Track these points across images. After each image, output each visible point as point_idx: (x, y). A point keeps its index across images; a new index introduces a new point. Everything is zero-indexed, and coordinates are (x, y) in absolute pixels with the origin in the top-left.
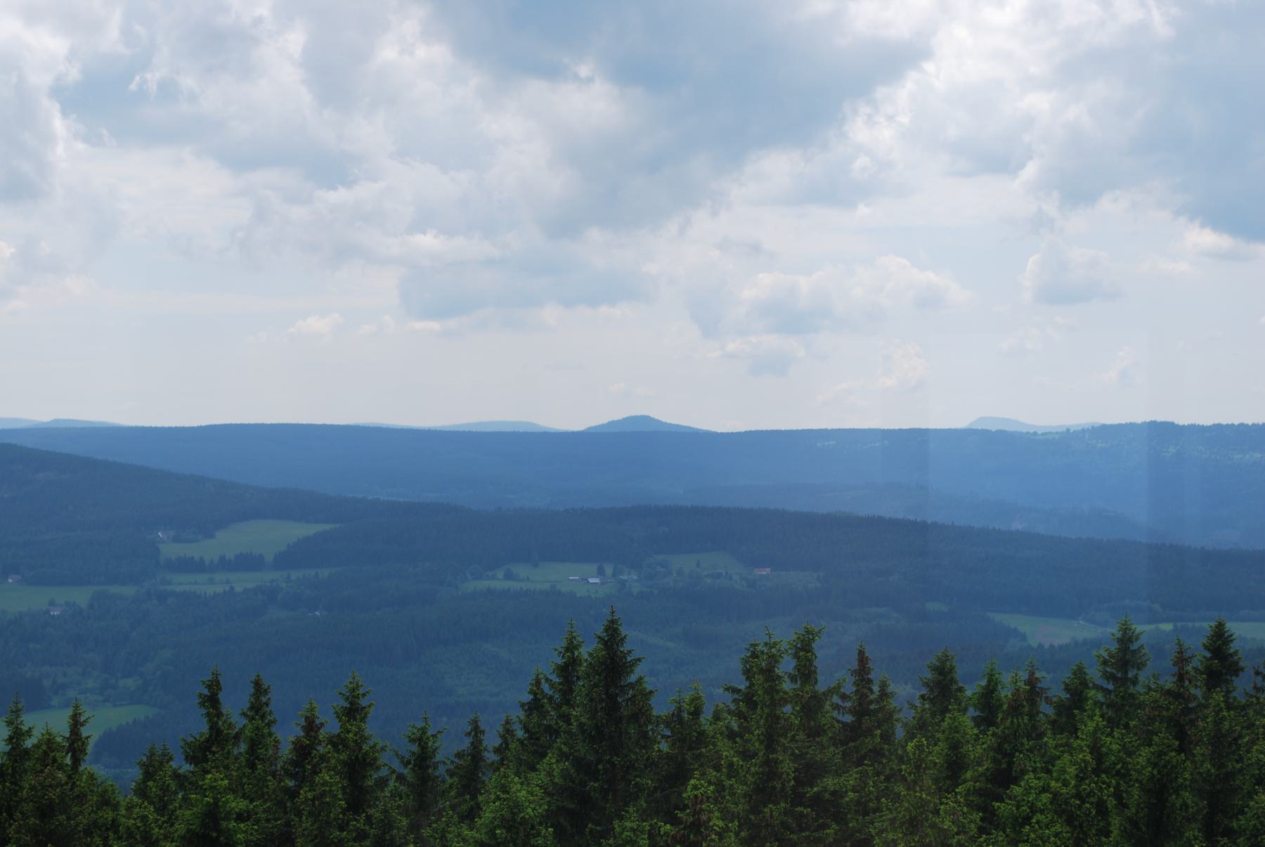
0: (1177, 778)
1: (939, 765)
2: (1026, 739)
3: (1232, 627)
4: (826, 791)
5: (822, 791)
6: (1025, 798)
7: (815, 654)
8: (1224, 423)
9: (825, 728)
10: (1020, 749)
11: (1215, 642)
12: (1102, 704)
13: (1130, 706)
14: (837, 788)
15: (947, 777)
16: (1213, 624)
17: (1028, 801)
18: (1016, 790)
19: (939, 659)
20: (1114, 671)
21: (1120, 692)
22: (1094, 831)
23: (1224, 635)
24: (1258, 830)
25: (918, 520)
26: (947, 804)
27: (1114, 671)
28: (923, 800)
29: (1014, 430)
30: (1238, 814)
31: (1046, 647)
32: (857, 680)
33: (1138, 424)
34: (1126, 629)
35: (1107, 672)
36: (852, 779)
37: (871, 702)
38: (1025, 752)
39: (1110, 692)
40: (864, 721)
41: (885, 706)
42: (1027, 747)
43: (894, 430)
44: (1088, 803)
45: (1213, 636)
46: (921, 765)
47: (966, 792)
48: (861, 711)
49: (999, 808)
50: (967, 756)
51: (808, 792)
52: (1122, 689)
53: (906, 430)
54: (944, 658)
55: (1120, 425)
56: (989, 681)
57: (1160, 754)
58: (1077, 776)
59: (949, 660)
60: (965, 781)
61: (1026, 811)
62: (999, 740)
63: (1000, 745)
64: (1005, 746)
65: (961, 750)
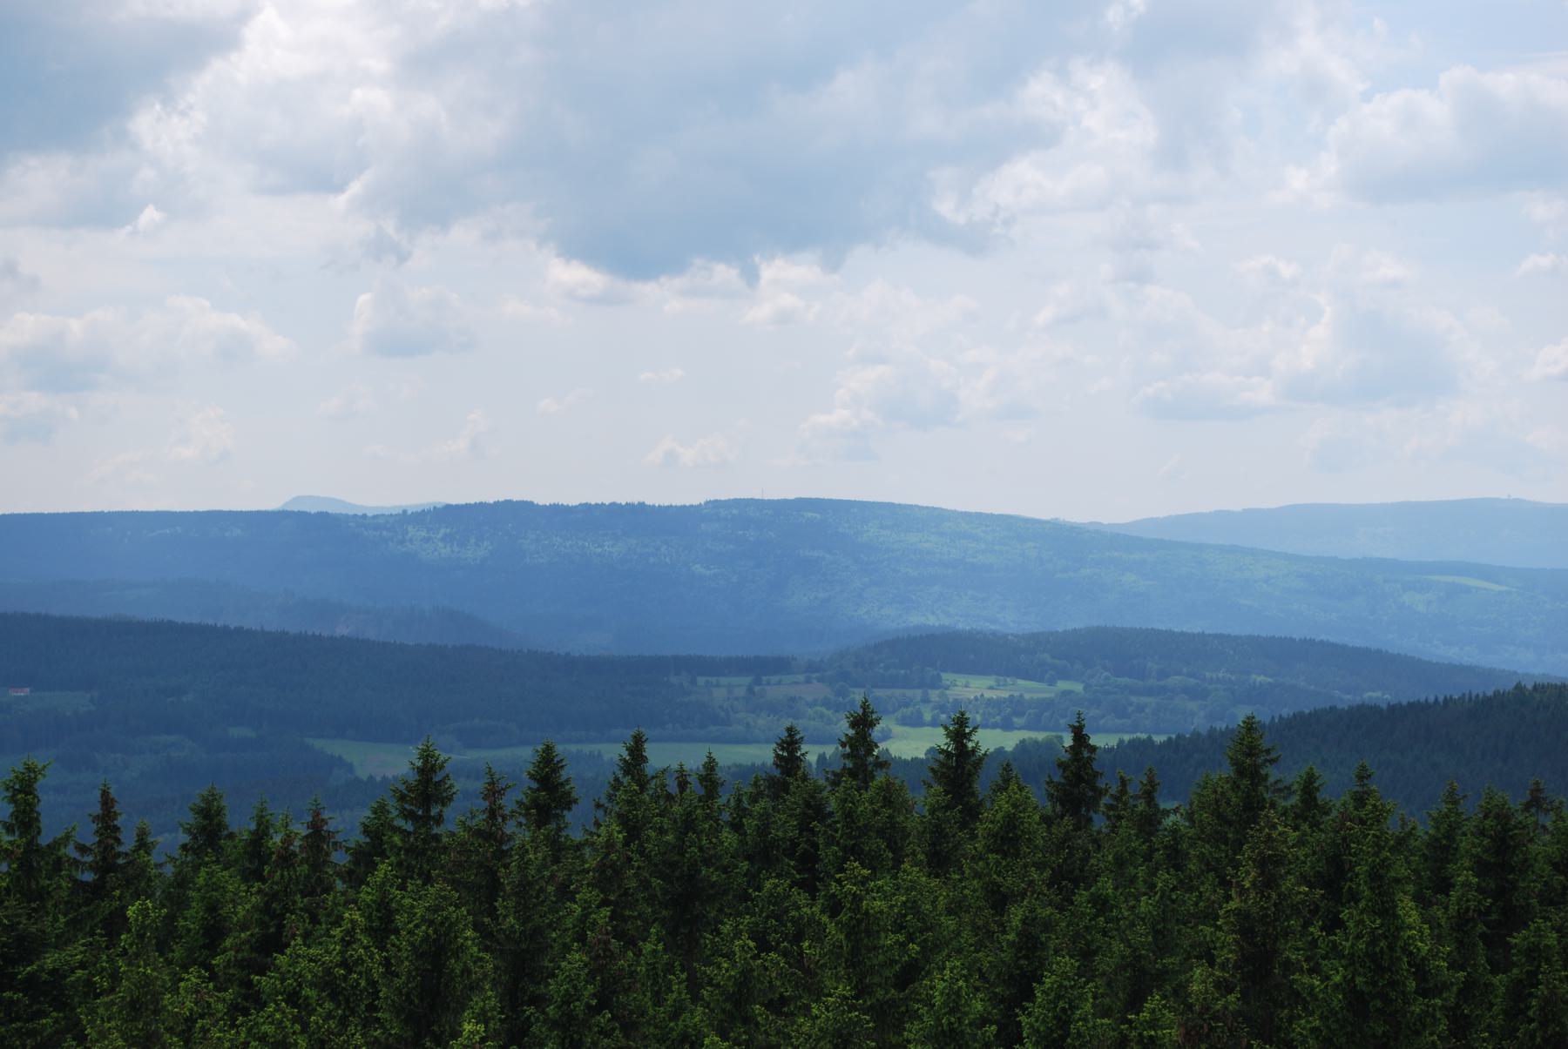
0: (456, 937)
1: (193, 931)
2: (299, 896)
3: (559, 749)
4: (43, 970)
5: (37, 971)
6: (291, 969)
7: (38, 797)
8: (593, 503)
9: (50, 889)
10: (292, 908)
11: (542, 769)
12: (400, 849)
13: (434, 850)
14: (57, 965)
15: (204, 947)
16: (540, 748)
17: (295, 973)
18: (281, 960)
19: (204, 799)
20: (413, 808)
21: (421, 834)
22: (363, 1007)
23: (552, 760)
24: (571, 996)
25: (219, 625)
26: (188, 980)
27: (413, 808)
28: (147, 976)
29: (338, 512)
30: (548, 977)
31: (378, 779)
32: (101, 828)
33: (490, 505)
34: (428, 756)
35: (405, 809)
36: (76, 951)
37: (119, 855)
38: (298, 912)
39: (408, 834)
40: (108, 879)
41: (135, 859)
42: (300, 905)
43: (188, 512)
44: (355, 972)
45: (540, 762)
46: (145, 934)
47: (225, 964)
48: (106, 865)
49: (259, 982)
50: (228, 919)
51: (20, 973)
52: (423, 830)
53: (203, 512)
54: (211, 798)
55: (467, 506)
56: (259, 825)
57: (436, 909)
58: (343, 939)
59: (216, 799)
60: (225, 950)
61: (292, 984)
62: (266, 899)
63: (267, 904)
64: (274, 905)
65: (221, 912)
